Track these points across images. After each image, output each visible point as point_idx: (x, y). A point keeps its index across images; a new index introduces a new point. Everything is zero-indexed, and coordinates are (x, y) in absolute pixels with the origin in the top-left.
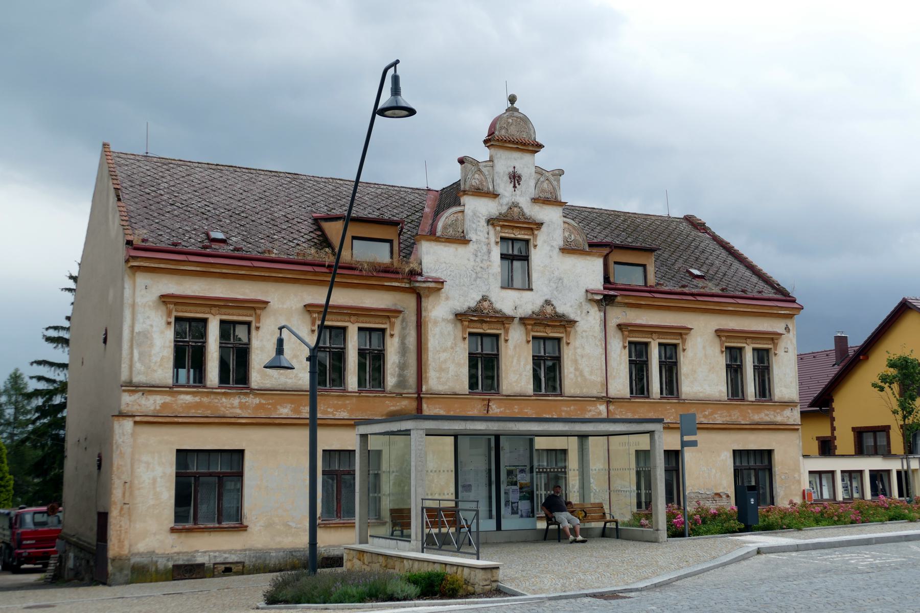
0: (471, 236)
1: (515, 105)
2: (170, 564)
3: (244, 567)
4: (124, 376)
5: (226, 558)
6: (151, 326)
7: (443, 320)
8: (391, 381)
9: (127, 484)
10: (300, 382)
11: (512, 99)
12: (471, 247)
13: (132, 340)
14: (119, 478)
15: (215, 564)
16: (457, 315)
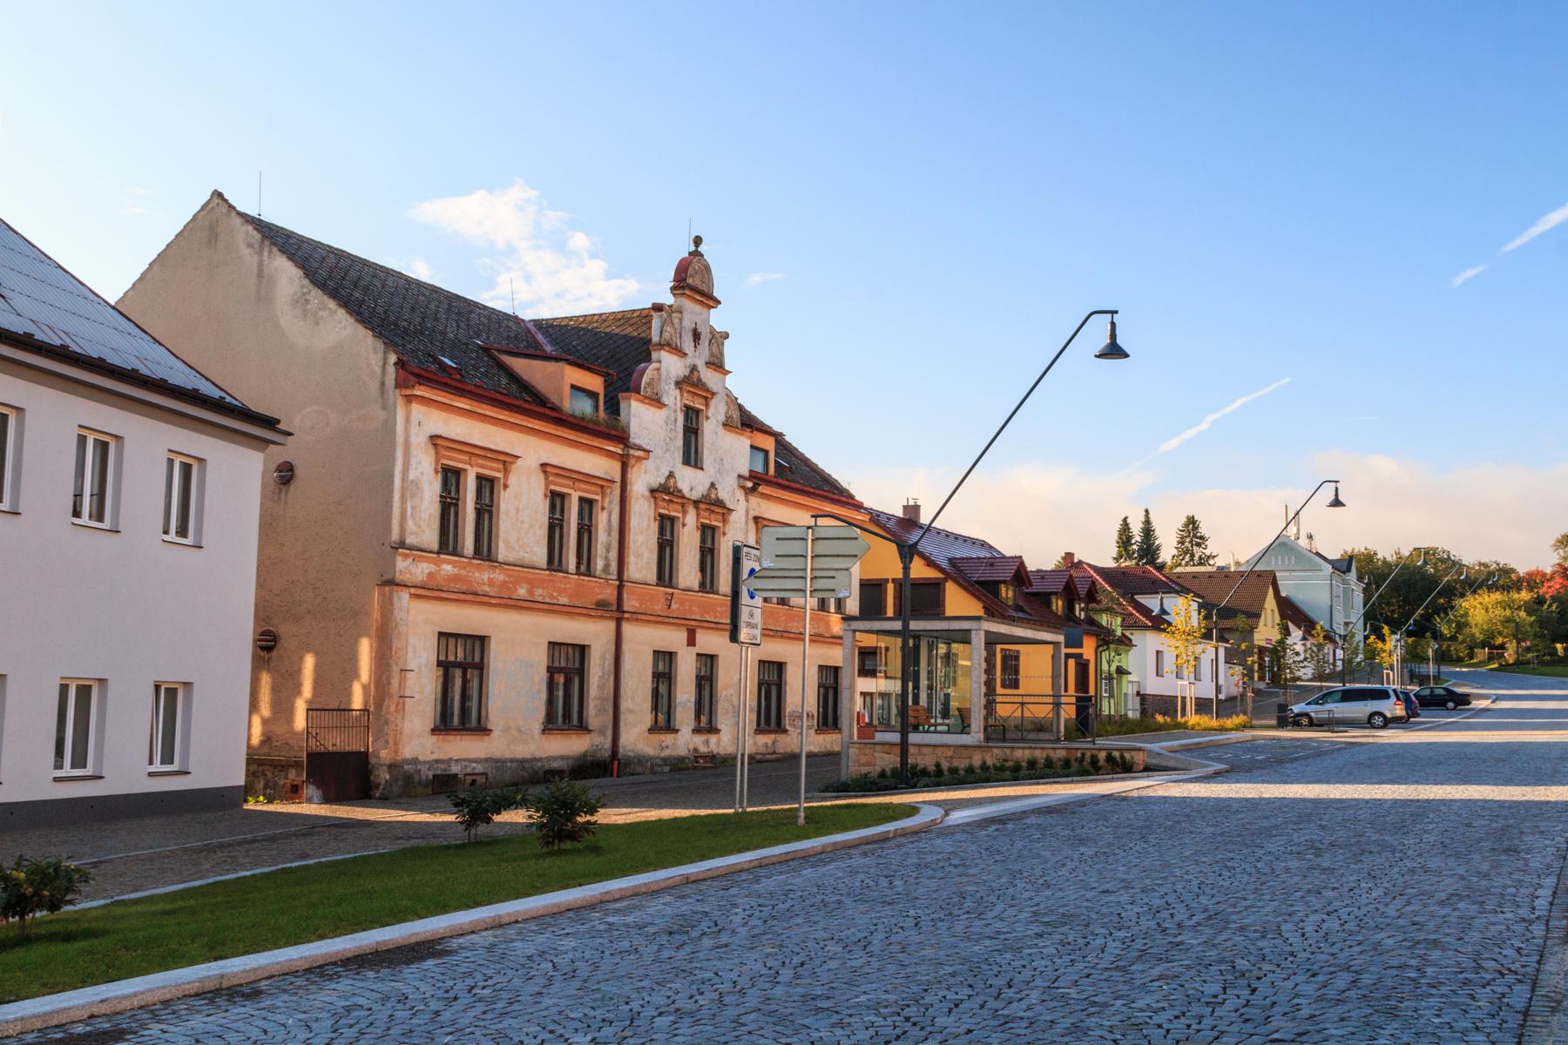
0: (665, 400)
1: (699, 249)
2: (431, 774)
3: (487, 779)
4: (395, 536)
5: (474, 768)
6: (422, 474)
7: (643, 496)
8: (599, 564)
9: (409, 675)
10: (534, 558)
11: (698, 241)
12: (664, 412)
13: (403, 489)
14: (397, 665)
15: (465, 775)
16: (652, 491)
